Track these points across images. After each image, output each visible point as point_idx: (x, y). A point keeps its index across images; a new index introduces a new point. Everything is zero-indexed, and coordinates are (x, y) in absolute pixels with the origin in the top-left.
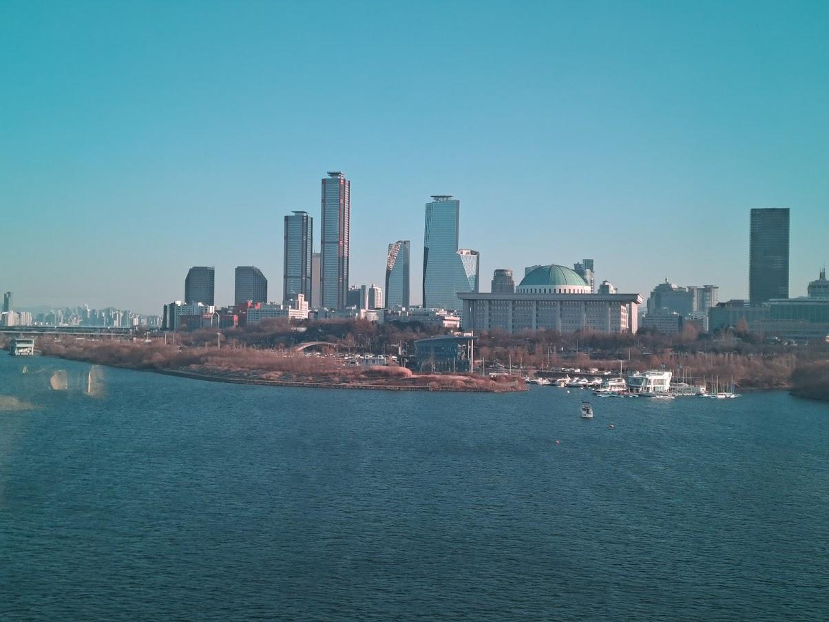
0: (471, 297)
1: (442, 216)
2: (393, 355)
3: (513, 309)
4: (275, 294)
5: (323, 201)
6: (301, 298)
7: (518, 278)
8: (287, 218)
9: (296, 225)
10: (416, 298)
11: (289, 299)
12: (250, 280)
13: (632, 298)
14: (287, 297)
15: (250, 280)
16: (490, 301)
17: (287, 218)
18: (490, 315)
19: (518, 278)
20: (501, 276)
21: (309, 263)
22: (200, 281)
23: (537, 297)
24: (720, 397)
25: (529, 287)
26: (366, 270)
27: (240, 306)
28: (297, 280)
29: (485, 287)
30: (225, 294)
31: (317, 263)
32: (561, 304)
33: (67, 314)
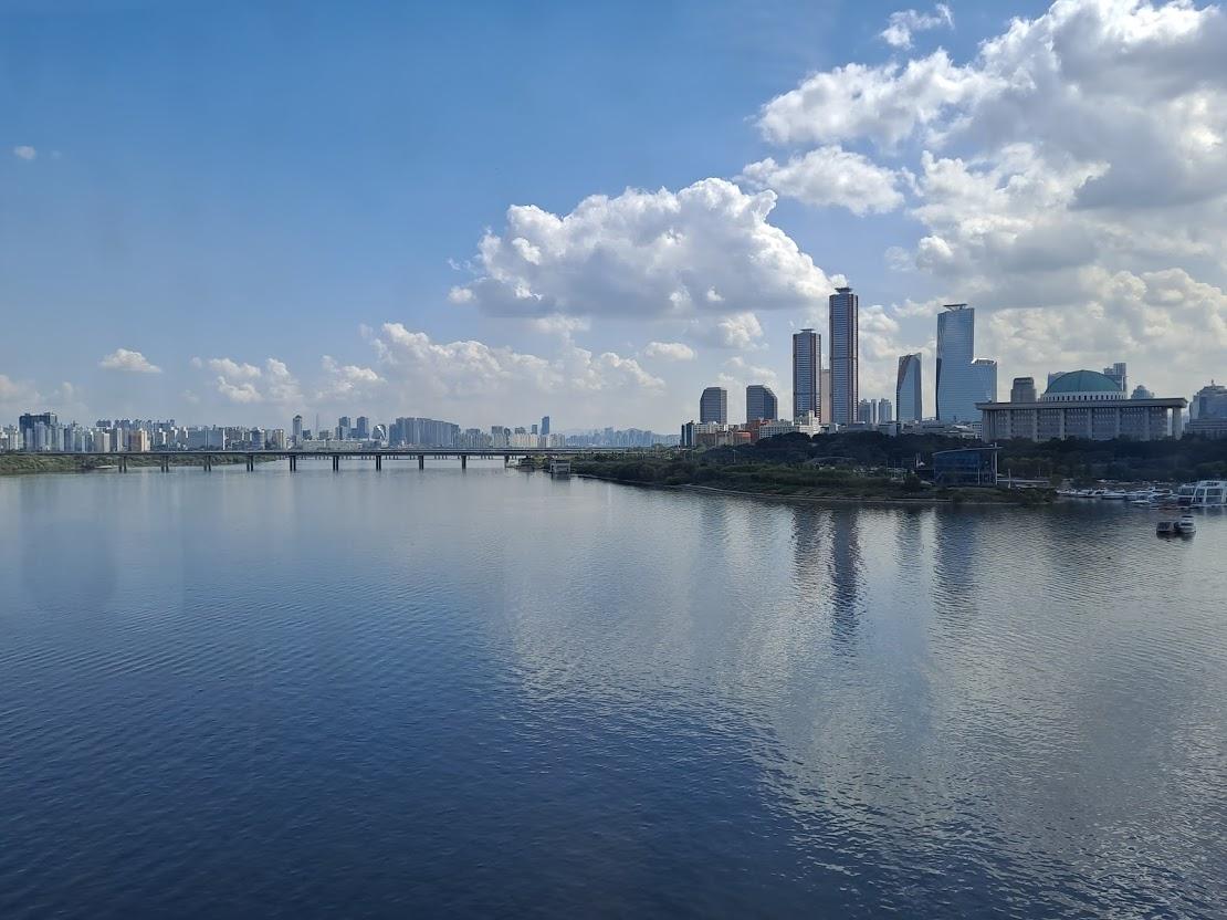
0: (988, 407)
1: (956, 324)
2: (872, 466)
3: (1121, 416)
4: (785, 411)
5: (795, 356)
6: (811, 414)
7: (1041, 386)
8: (795, 336)
9: (804, 344)
10: (929, 411)
11: (799, 413)
12: (761, 400)
13: (1177, 404)
14: (796, 414)
15: (761, 400)
16: (1012, 411)
17: (795, 336)
18: (1038, 424)
19: (1041, 386)
20: (1023, 385)
21: (817, 381)
22: (713, 400)
23: (1064, 405)
24: (137, 359)
25: (1052, 395)
26: (875, 383)
27: (752, 425)
28: (805, 398)
29: (1004, 395)
30: (737, 413)
31: (826, 379)
32: (1065, 412)
33: (218, 432)
